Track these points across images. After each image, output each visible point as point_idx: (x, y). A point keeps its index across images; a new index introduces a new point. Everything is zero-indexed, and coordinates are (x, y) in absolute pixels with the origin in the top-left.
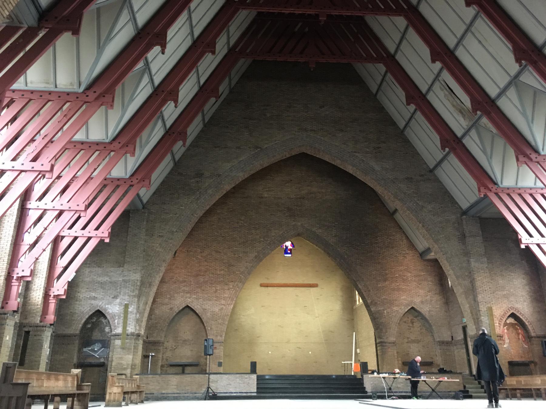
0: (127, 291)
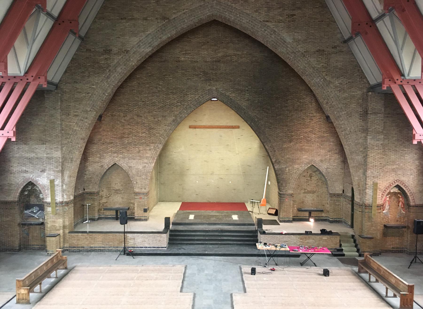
0: (52, 167)
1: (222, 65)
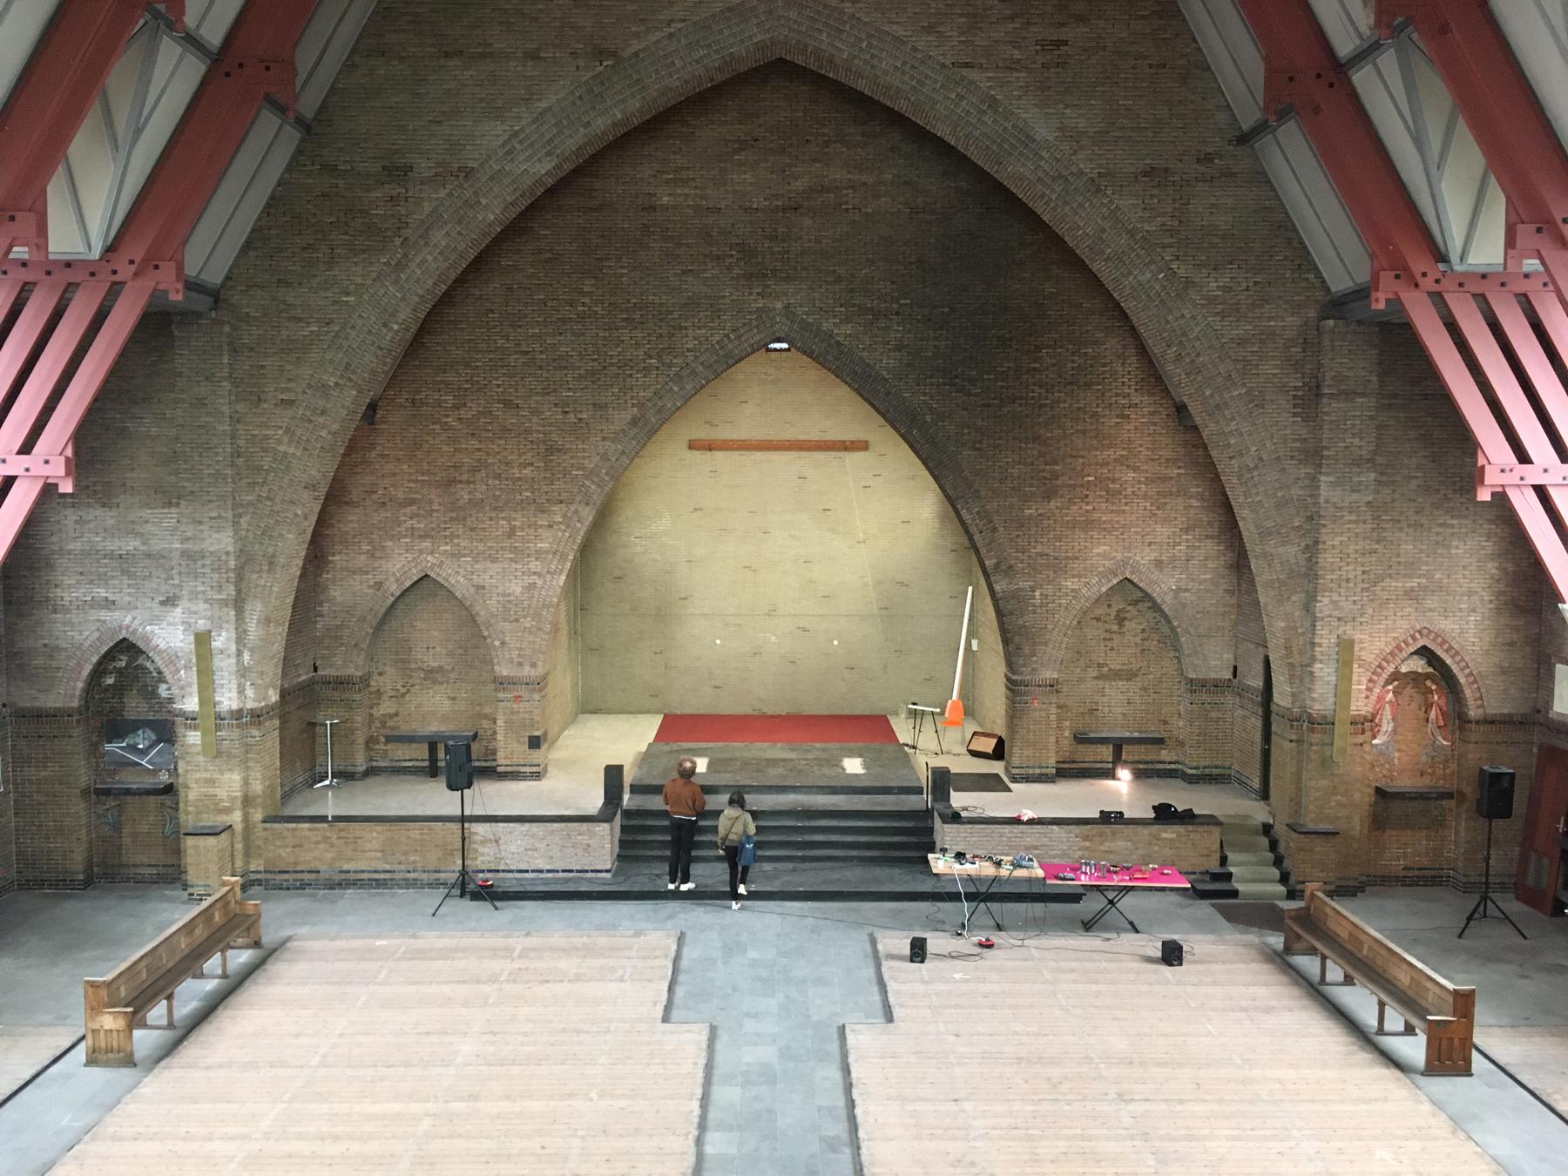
0: (201, 588)
1: (807, 222)
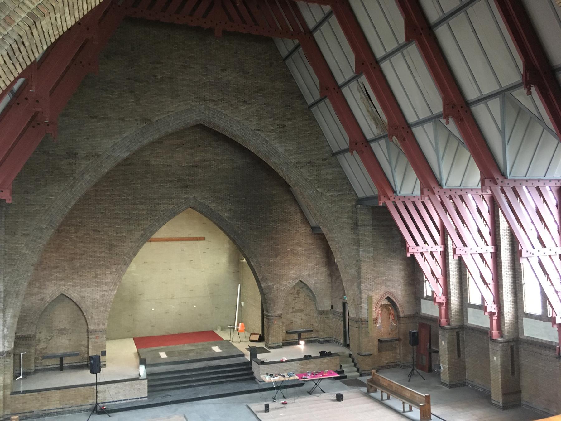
1: (200, 171)
